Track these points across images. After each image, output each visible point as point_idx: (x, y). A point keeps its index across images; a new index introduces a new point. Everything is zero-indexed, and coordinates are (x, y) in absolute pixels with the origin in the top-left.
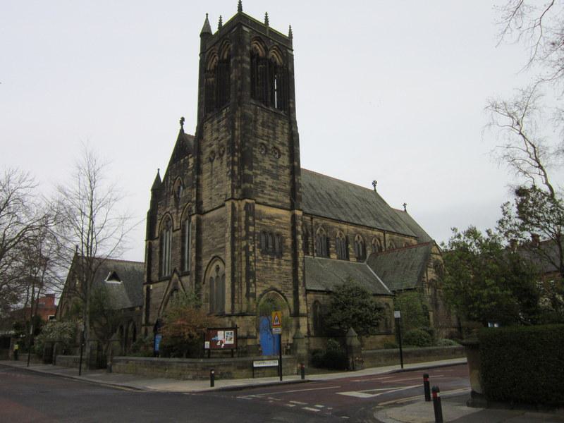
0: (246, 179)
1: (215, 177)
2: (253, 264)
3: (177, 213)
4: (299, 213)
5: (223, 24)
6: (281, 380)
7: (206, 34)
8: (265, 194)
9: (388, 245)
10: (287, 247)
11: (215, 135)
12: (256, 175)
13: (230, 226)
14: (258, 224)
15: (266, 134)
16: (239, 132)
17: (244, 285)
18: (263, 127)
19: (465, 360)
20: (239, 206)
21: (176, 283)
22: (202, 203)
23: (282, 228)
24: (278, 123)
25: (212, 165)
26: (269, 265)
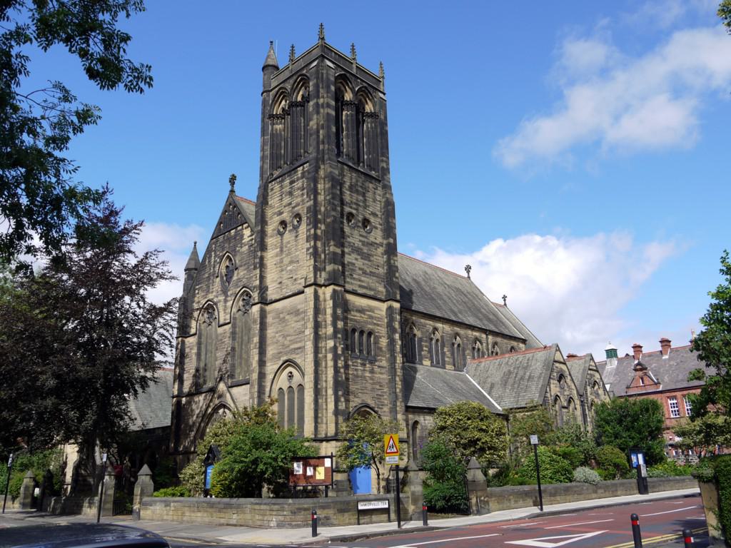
1: (287, 255)
2: (342, 370)
3: (226, 301)
8: (354, 279)
10: (380, 349)
13: (311, 320)
19: (697, 490)
22: (267, 289)
23: (375, 324)
24: (369, 187)
26: (360, 373)
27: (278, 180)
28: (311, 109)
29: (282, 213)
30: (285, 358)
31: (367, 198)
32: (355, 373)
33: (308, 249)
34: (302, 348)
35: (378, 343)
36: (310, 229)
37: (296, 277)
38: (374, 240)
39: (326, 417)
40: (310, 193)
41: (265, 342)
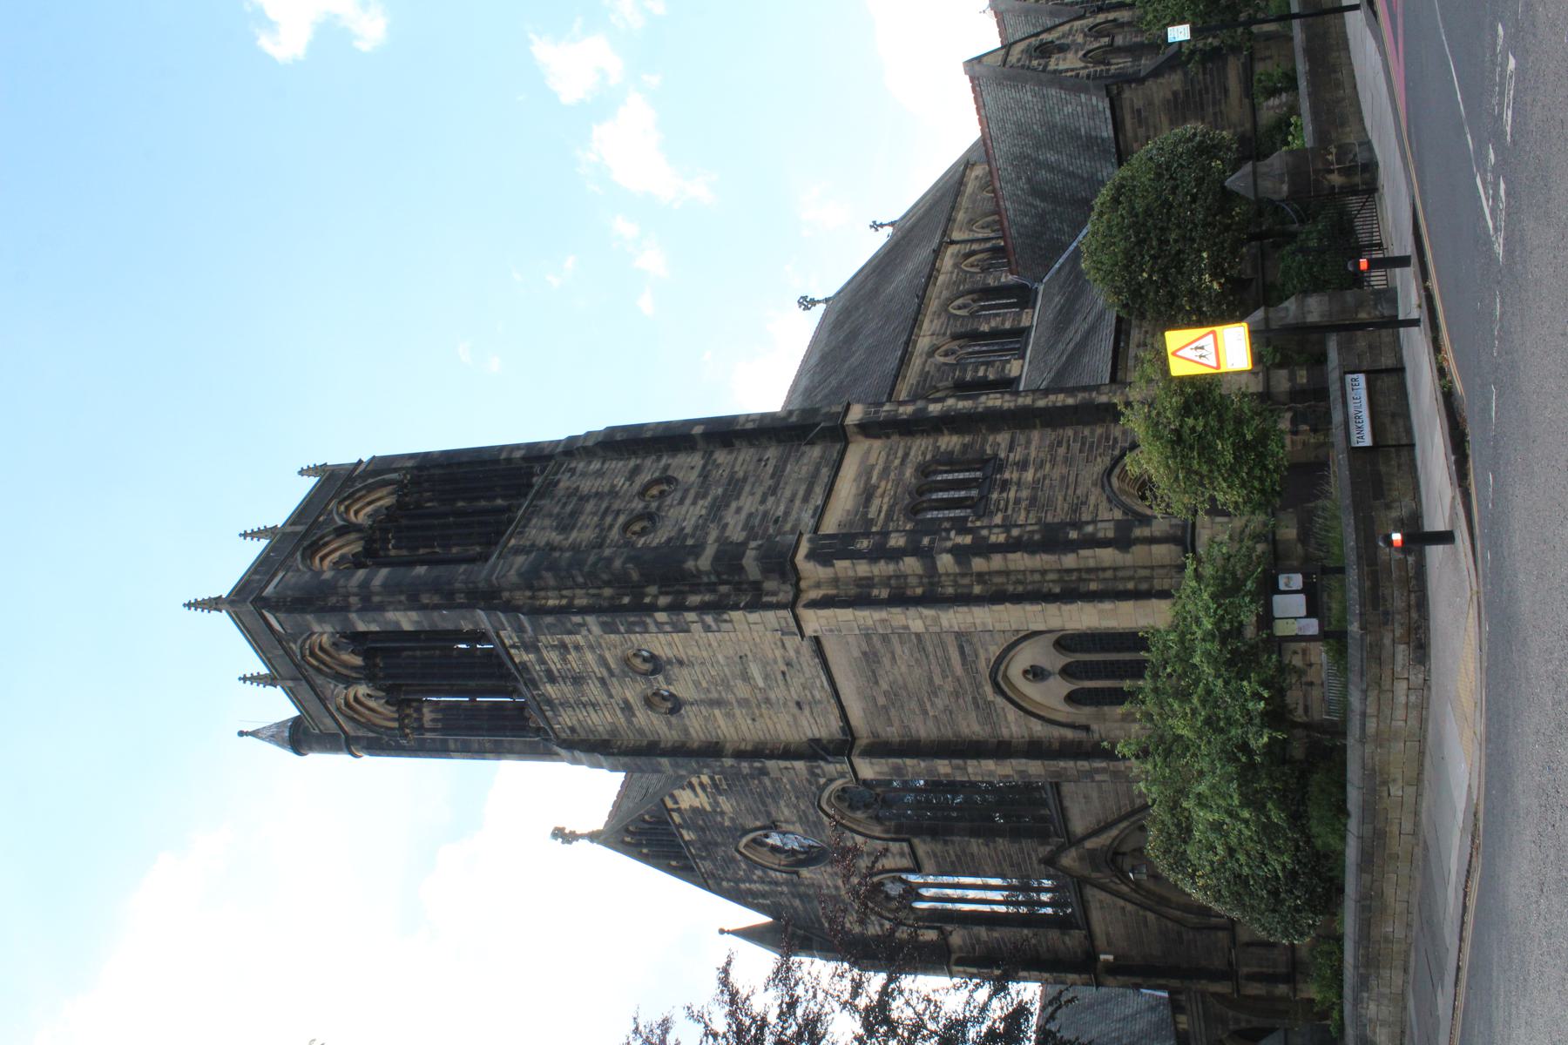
0: (730, 557)
1: (729, 688)
2: (1015, 532)
4: (856, 414)
5: (264, 670)
6: (1415, 323)
7: (298, 737)
11: (593, 691)
16: (579, 592)
18: (573, 528)
20: (818, 585)
21: (1092, 857)
24: (568, 488)
26: (1025, 494)
27: (549, 714)
28: (374, 628)
29: (626, 702)
30: (988, 689)
31: (594, 490)
32: (1024, 504)
33: (707, 629)
34: (962, 638)
35: (952, 452)
36: (658, 624)
37: (780, 661)
38: (696, 473)
39: (1135, 568)
40: (569, 626)
41: (949, 742)
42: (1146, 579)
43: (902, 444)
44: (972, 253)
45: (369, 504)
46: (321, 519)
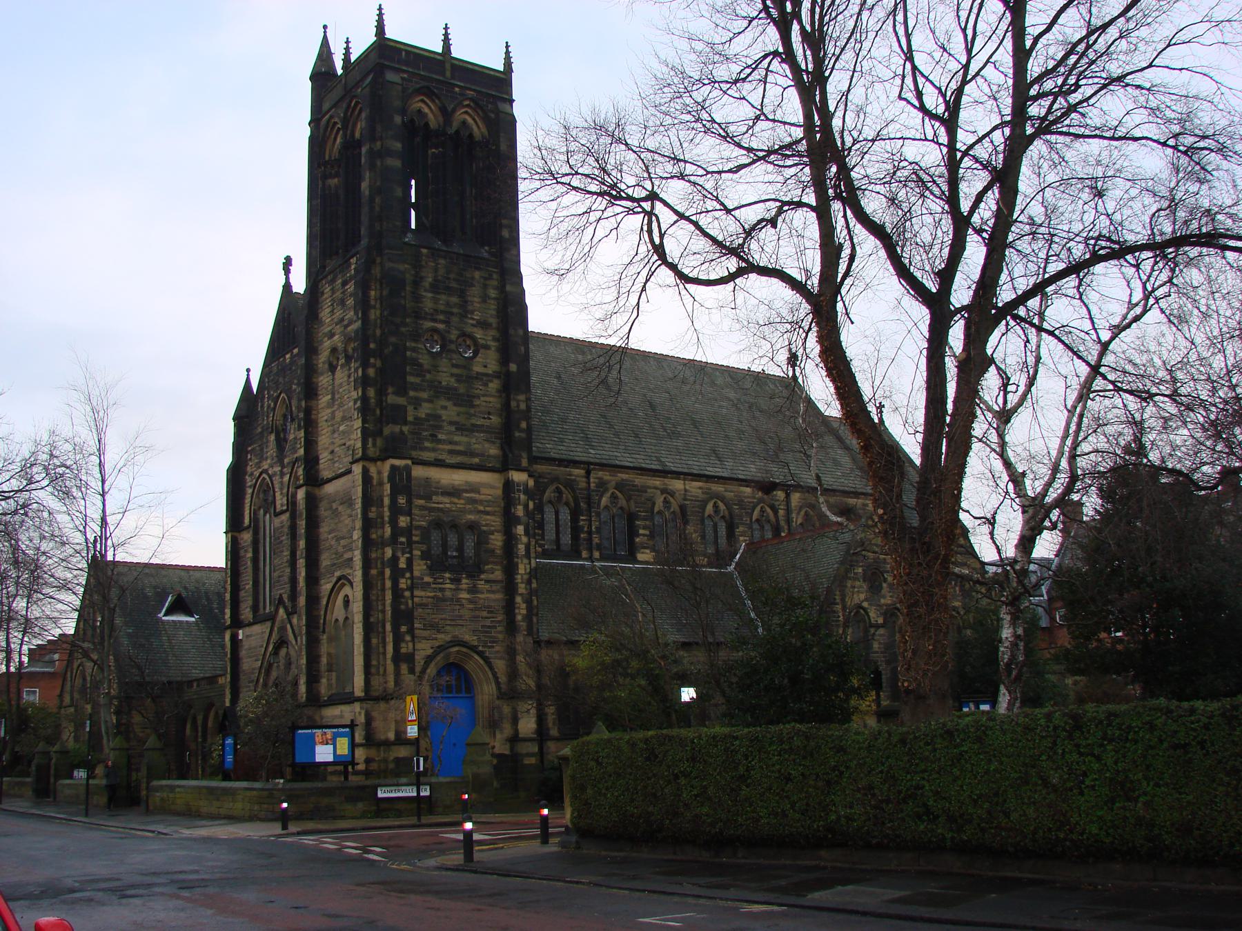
2: (407, 594)
3: (282, 474)
5: (353, 58)
7: (322, 76)
8: (439, 441)
9: (797, 519)
11: (338, 313)
12: (417, 403)
14: (423, 508)
15: (442, 308)
16: (378, 312)
17: (390, 638)
20: (379, 473)
21: (283, 629)
22: (317, 460)
24: (473, 278)
25: (333, 380)
26: (448, 594)
30: (338, 574)
31: (469, 298)
32: (440, 594)
42: (378, 674)
43: (497, 509)
44: (775, 511)
45: (474, 119)
46: (457, 89)
